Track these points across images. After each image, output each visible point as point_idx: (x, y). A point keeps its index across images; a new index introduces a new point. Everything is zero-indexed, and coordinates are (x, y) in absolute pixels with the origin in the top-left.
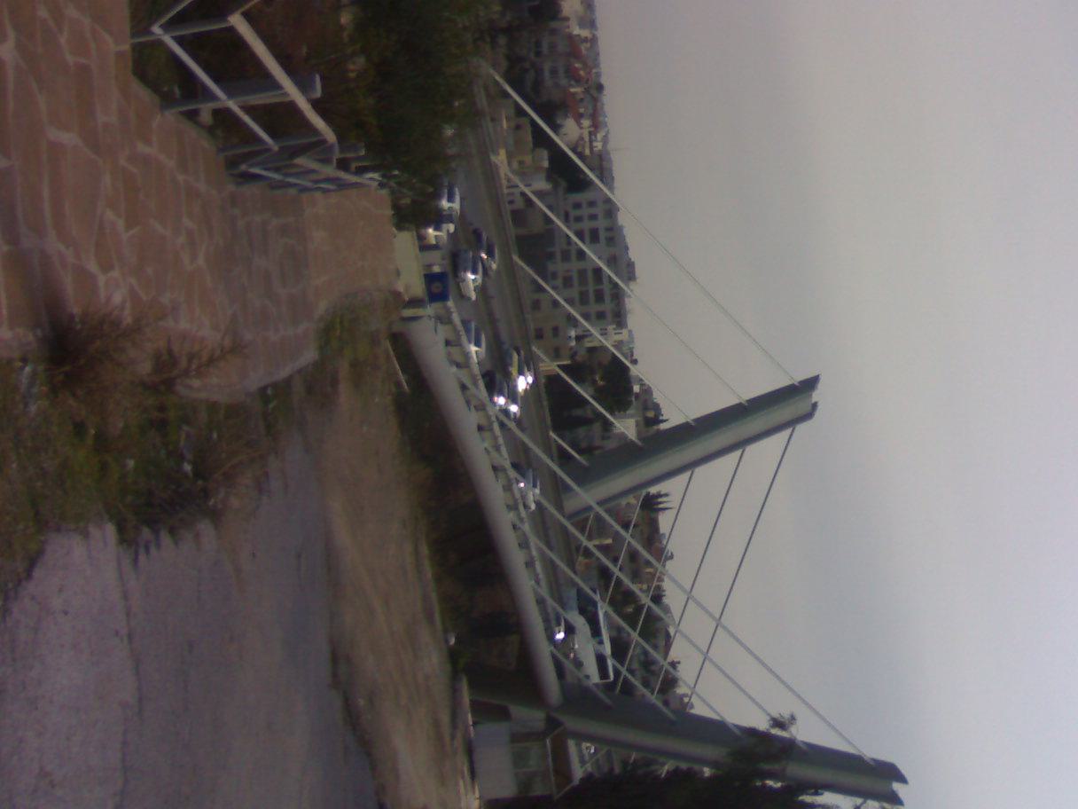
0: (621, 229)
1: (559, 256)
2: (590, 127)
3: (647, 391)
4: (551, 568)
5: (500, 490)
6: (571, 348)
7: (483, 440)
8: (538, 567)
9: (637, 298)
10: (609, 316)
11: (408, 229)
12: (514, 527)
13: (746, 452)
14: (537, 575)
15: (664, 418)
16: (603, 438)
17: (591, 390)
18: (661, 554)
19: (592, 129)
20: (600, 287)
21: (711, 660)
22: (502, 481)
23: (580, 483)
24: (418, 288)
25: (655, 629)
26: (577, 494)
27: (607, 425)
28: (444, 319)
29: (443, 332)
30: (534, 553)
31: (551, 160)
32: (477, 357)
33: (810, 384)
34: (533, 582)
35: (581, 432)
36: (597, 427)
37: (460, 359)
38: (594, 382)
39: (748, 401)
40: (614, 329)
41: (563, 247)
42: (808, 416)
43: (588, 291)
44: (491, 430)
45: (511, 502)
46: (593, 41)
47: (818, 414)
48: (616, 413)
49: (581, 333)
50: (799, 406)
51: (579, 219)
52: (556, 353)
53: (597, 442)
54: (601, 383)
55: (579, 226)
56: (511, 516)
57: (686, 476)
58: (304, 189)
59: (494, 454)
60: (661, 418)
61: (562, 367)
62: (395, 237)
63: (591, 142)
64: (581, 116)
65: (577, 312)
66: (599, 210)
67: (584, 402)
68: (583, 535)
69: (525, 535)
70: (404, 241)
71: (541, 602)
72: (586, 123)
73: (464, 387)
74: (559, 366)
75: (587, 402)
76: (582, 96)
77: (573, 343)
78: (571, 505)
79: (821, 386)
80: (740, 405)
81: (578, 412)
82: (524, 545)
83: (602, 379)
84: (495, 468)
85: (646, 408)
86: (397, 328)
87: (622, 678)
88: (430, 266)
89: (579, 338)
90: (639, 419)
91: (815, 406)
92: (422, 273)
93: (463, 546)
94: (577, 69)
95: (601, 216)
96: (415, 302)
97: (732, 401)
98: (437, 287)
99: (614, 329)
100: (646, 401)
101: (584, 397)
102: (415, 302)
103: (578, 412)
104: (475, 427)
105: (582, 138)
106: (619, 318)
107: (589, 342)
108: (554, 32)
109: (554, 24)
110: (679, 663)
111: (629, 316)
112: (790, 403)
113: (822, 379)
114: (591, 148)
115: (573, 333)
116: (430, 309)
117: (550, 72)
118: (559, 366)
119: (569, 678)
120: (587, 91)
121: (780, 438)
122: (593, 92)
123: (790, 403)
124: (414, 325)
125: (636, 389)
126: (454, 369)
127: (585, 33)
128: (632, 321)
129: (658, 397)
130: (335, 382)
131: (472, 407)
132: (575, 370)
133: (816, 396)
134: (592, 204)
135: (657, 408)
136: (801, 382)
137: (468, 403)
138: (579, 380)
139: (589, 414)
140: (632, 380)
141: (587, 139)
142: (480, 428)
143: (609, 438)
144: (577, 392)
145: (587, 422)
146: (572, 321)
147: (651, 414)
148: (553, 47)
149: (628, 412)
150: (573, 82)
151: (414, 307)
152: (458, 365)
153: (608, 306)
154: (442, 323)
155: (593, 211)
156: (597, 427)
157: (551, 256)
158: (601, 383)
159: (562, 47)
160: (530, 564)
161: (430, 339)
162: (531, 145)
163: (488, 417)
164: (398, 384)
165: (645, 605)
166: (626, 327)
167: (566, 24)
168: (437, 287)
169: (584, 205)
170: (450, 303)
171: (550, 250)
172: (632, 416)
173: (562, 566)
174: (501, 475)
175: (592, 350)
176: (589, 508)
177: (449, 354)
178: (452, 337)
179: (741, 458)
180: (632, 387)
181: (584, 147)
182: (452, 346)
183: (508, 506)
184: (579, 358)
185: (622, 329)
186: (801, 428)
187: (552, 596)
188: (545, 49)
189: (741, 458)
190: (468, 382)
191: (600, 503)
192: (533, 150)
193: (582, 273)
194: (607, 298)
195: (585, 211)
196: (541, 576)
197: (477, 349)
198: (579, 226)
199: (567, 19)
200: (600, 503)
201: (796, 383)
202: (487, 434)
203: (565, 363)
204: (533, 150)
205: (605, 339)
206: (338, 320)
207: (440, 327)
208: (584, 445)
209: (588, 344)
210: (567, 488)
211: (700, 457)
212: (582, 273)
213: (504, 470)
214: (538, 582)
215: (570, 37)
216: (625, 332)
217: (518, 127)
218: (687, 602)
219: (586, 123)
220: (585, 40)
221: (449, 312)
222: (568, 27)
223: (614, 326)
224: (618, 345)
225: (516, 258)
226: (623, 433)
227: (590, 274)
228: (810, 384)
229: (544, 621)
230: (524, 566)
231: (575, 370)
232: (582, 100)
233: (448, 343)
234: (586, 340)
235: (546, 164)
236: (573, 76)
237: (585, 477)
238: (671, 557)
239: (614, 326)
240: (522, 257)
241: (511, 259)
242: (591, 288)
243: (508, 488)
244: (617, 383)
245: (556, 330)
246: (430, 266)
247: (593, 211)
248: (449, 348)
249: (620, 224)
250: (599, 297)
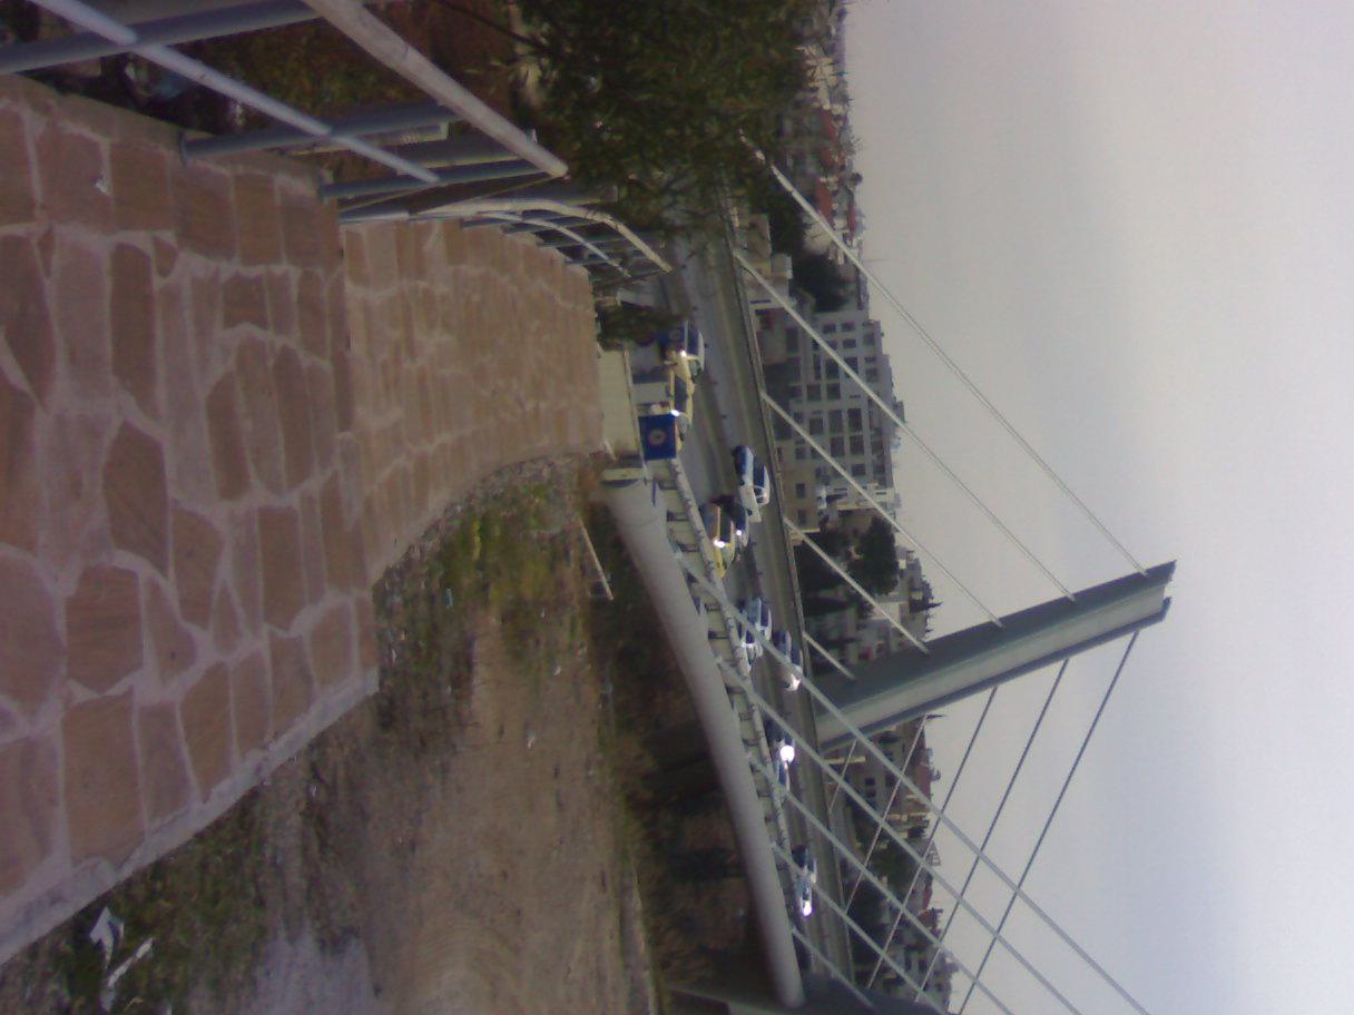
0: (886, 359)
2: (844, 229)
3: (914, 566)
4: (797, 821)
6: (821, 513)
8: (782, 821)
10: (869, 470)
12: (752, 768)
14: (779, 833)
15: (935, 601)
16: (858, 627)
18: (923, 774)
19: (848, 231)
21: (992, 931)
23: (839, 702)
24: (632, 439)
26: (834, 717)
27: (864, 609)
28: (667, 483)
29: (665, 501)
30: (778, 803)
33: (1163, 573)
34: (774, 844)
35: (831, 619)
37: (686, 539)
38: (849, 555)
39: (1076, 595)
40: (877, 488)
41: (812, 374)
42: (1157, 616)
45: (749, 735)
48: (876, 595)
49: (833, 493)
51: (850, 344)
52: (802, 520)
53: (851, 633)
54: (856, 556)
55: (851, 353)
56: (750, 756)
57: (984, 695)
58: (358, 186)
59: (732, 672)
60: (931, 601)
61: (810, 536)
62: (599, 357)
64: (834, 214)
65: (825, 461)
66: (858, 334)
67: (839, 580)
69: (766, 780)
70: (614, 367)
72: (840, 223)
73: (690, 579)
75: (841, 580)
76: (836, 188)
77: (824, 506)
78: (826, 730)
79: (1176, 576)
83: (857, 552)
84: (729, 690)
85: (912, 589)
86: (595, 497)
87: (879, 964)
88: (648, 405)
89: (830, 499)
90: (902, 603)
91: (1167, 602)
93: (674, 789)
95: (859, 342)
96: (627, 459)
97: (1054, 594)
98: (657, 437)
99: (877, 488)
100: (911, 581)
102: (627, 459)
104: (706, 636)
106: (882, 474)
107: (842, 504)
110: (941, 911)
111: (894, 470)
112: (1136, 597)
115: (823, 493)
116: (647, 470)
117: (896, 70)
119: (814, 969)
120: (840, 182)
121: (1118, 645)
122: (848, 184)
123: (1136, 597)
125: (902, 564)
126: (679, 555)
128: (897, 475)
129: (929, 574)
130: (464, 663)
132: (828, 540)
133: (1169, 590)
134: (848, 327)
135: (926, 588)
137: (696, 601)
138: (832, 553)
139: (840, 594)
142: (712, 636)
143: (865, 627)
145: (839, 607)
146: (824, 475)
147: (918, 596)
149: (891, 594)
152: (684, 548)
153: (868, 458)
154: (662, 488)
155: (850, 335)
156: (851, 613)
157: (795, 393)
158: (856, 556)
160: (770, 819)
161: (646, 512)
162: (770, 250)
163: (724, 621)
164: (598, 588)
166: (891, 485)
168: (657, 437)
169: (839, 328)
170: (676, 461)
171: (793, 384)
173: (812, 819)
174: (738, 699)
175: (846, 514)
176: (849, 736)
177: (671, 532)
178: (676, 509)
179: (1061, 673)
180: (897, 563)
183: (745, 742)
184: (829, 525)
185: (886, 487)
186: (1146, 633)
188: (788, 125)
189: (1061, 673)
190: (696, 572)
191: (864, 730)
194: (868, 448)
195: (840, 336)
196: (785, 834)
198: (851, 353)
199: (815, 90)
200: (864, 730)
201: (1143, 573)
202: (720, 644)
203: (813, 531)
206: (477, 526)
208: (834, 635)
209: (841, 506)
210: (822, 710)
211: (1010, 668)
212: (835, 415)
213: (743, 693)
214: (780, 844)
216: (889, 491)
218: (1014, 898)
219: (840, 223)
220: (838, 118)
221: (674, 474)
224: (884, 505)
225: (764, 395)
227: (845, 416)
228: (1163, 573)
229: (785, 893)
231: (828, 540)
232: (835, 193)
233: (670, 517)
234: (838, 501)
235: (789, 274)
236: (827, 167)
237: (845, 694)
239: (877, 484)
241: (758, 397)
242: (847, 435)
244: (878, 553)
245: (801, 488)
246: (648, 405)
247: (850, 335)
248: (673, 525)
249: (884, 352)
250: (857, 447)
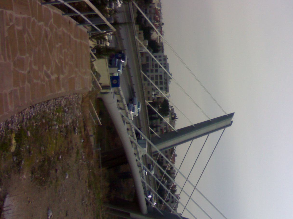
0: (168, 64)
1: (150, 71)
3: (173, 110)
5: (133, 149)
6: (153, 98)
7: (129, 134)
9: (172, 85)
11: (103, 58)
13: (209, 135)
16: (161, 123)
17: (158, 110)
20: (161, 80)
22: (134, 146)
25: (171, 172)
27: (161, 119)
29: (117, 97)
31: (149, 43)
32: (133, 115)
33: (231, 115)
36: (159, 120)
38: (159, 107)
40: (165, 92)
42: (230, 125)
43: (158, 81)
44: (131, 130)
46: (160, 10)
47: (232, 124)
49: (156, 93)
50: (228, 122)
53: (159, 124)
54: (160, 107)
60: (176, 117)
63: (160, 39)
67: (155, 113)
68: (165, 174)
71: (143, 183)
74: (149, 103)
77: (153, 96)
79: (234, 116)
80: (209, 121)
81: (153, 116)
82: (139, 166)
83: (161, 106)
84: (132, 142)
85: (172, 115)
86: (99, 96)
88: (113, 74)
89: (155, 95)
91: (232, 122)
92: (109, 76)
94: (157, 18)
98: (115, 82)
101: (156, 112)
103: (153, 116)
105: (157, 38)
108: (151, 7)
109: (151, 5)
113: (235, 113)
114: (160, 41)
115: (154, 93)
116: (112, 90)
118: (149, 103)
124: (106, 96)
125: (170, 109)
127: (159, 8)
128: (170, 90)
129: (176, 111)
131: (125, 123)
132: (154, 104)
133: (232, 119)
135: (175, 114)
136: (228, 115)
137: (124, 122)
139: (157, 116)
140: (169, 107)
141: (159, 38)
142: (128, 129)
144: (153, 110)
146: (154, 89)
147: (173, 116)
148: (150, 11)
150: (156, 22)
151: (106, 89)
153: (164, 86)
154: (116, 94)
157: (148, 71)
158: (160, 107)
159: (153, 11)
164: (98, 122)
165: (159, 153)
166: (168, 92)
167: (154, 5)
168: (115, 82)
171: (147, 69)
172: (168, 117)
174: (133, 144)
175: (158, 98)
178: (119, 99)
181: (158, 40)
182: (120, 102)
183: (135, 154)
184: (155, 101)
186: (227, 129)
187: (147, 182)
192: (144, 40)
193: (157, 76)
194: (163, 84)
197: (133, 112)
199: (154, 4)
202: (130, 132)
204: (144, 40)
205: (164, 94)
207: (115, 95)
209: (157, 96)
212: (157, 76)
215: (155, 9)
217: (140, 33)
222: (155, 6)
223: (165, 92)
226: (165, 122)
227: (159, 77)
228: (231, 115)
230: (117, 101)
235: (147, 44)
238: (177, 156)
240: (143, 71)
242: (159, 80)
243: (136, 148)
244: (165, 107)
245: (149, 92)
248: (119, 103)
